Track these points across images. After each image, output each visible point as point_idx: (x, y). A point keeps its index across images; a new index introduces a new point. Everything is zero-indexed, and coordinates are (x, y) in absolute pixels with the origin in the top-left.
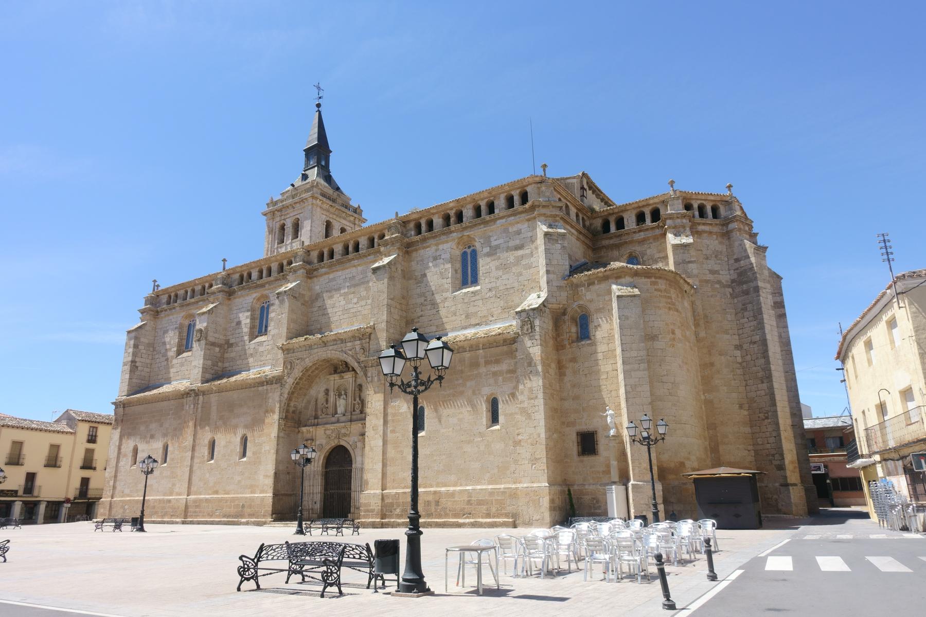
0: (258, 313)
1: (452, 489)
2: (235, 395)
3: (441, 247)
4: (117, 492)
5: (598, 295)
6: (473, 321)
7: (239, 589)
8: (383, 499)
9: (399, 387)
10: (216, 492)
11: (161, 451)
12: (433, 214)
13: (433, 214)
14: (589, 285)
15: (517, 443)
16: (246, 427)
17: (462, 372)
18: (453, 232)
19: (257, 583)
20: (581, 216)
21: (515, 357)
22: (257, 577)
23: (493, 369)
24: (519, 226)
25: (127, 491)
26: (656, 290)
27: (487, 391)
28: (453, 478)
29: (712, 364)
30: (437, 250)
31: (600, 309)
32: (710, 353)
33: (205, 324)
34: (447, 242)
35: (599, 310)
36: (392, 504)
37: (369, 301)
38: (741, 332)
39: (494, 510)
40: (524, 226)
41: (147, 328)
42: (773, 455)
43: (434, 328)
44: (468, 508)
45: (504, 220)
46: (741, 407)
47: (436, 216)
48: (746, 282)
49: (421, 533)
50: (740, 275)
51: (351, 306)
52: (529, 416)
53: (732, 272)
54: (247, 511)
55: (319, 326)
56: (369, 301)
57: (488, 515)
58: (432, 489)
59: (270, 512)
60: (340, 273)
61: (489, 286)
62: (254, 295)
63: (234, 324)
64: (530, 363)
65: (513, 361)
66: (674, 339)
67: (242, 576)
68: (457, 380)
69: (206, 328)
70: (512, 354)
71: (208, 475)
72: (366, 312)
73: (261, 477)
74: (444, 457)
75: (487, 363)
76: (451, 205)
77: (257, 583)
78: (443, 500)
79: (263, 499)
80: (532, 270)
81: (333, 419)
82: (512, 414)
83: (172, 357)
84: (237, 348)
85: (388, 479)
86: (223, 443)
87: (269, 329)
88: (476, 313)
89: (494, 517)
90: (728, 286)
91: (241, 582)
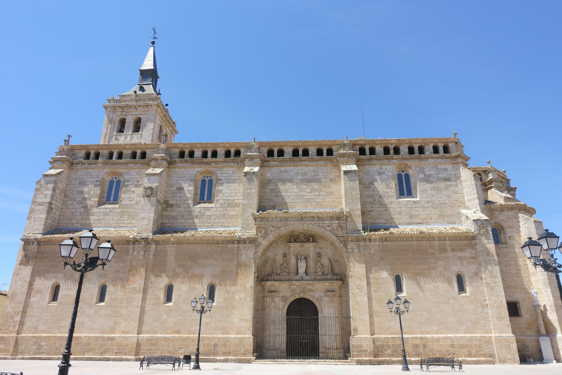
0: (199, 184)
1: (436, 336)
2: (199, 248)
3: (384, 167)
4: (25, 328)
5: (508, 218)
8: (374, 342)
9: (71, 266)
10: (178, 332)
13: (376, 144)
14: (501, 211)
16: (214, 276)
17: (433, 254)
18: (394, 159)
21: (475, 249)
23: (458, 255)
24: (446, 166)
25: (41, 327)
27: (455, 269)
30: (380, 169)
31: (510, 226)
33: (157, 184)
34: (390, 165)
35: (510, 227)
36: (383, 346)
39: (474, 351)
40: (450, 167)
41: (63, 175)
43: (383, 221)
45: (434, 160)
47: (379, 146)
49: (70, 365)
52: (492, 289)
54: (220, 349)
55: (272, 204)
57: (470, 355)
58: (419, 336)
59: (252, 351)
60: (292, 168)
61: (427, 199)
62: (199, 169)
63: (174, 189)
64: (488, 253)
65: (474, 252)
69: (156, 188)
70: (473, 247)
73: (236, 320)
74: (425, 312)
75: (453, 250)
76: (393, 141)
78: (429, 344)
79: (241, 340)
80: (458, 195)
81: (297, 277)
83: (92, 206)
84: (178, 209)
85: (376, 327)
88: (418, 215)
89: (474, 357)
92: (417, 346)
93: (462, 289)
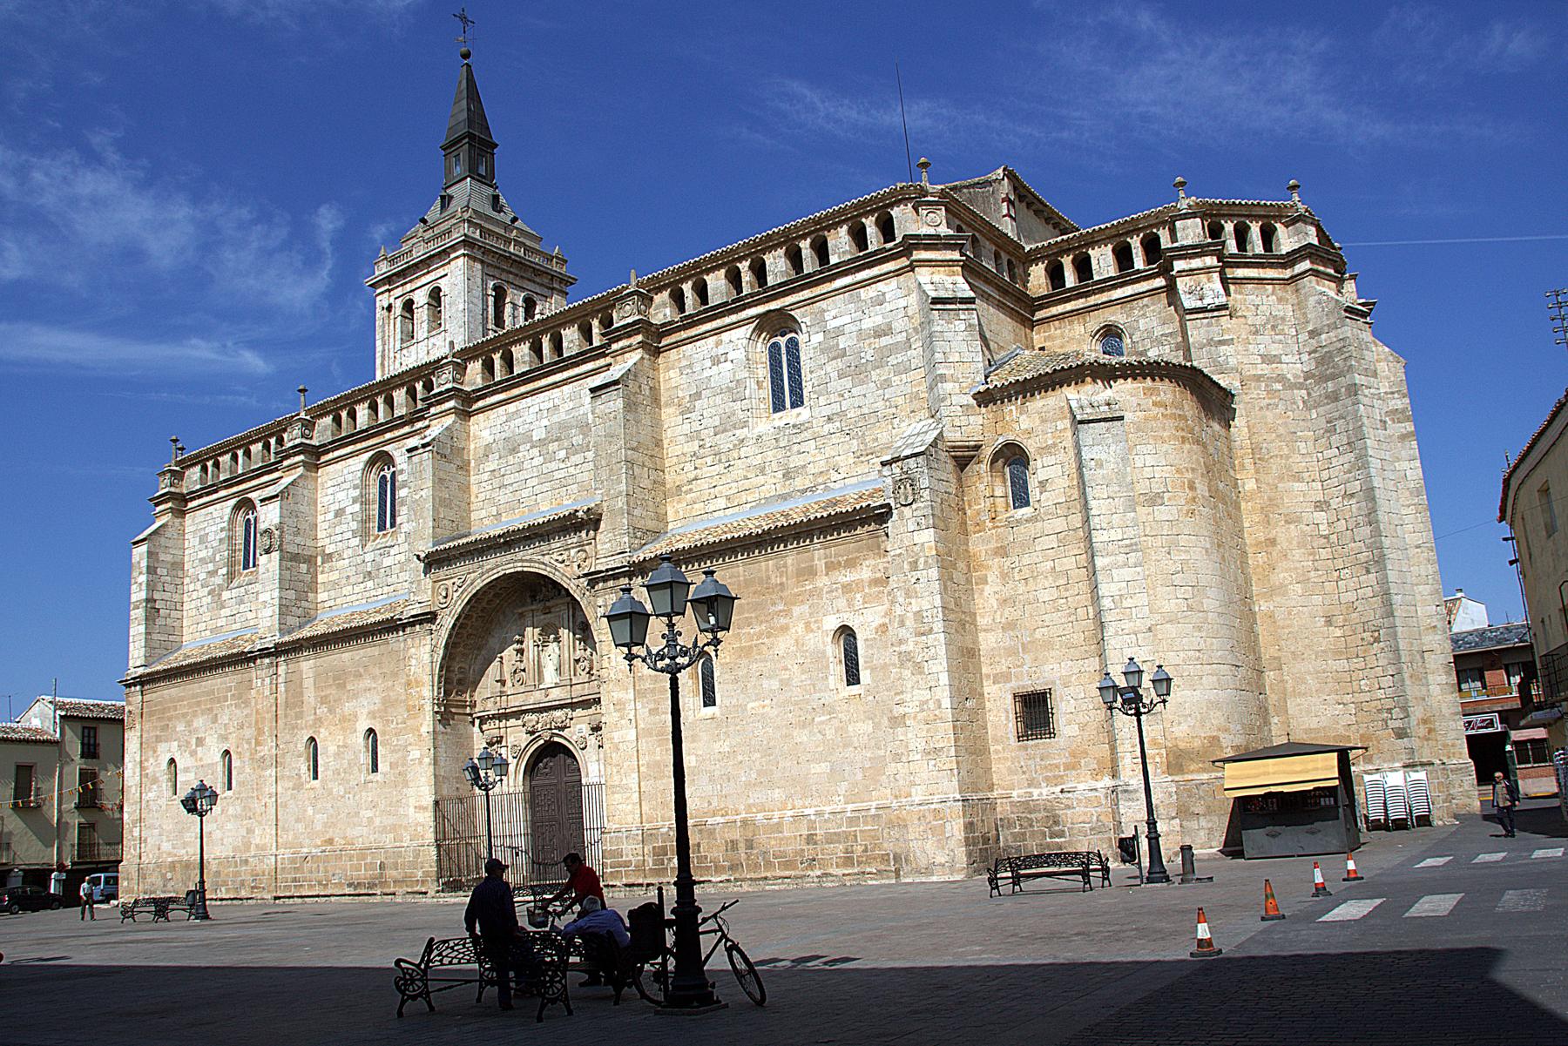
6: (799, 483)
7: (400, 1014)
9: (644, 660)
11: (220, 769)
12: (708, 271)
15: (897, 721)
19: (429, 1003)
20: (1005, 257)
22: (428, 993)
26: (1155, 404)
28: (778, 794)
29: (1273, 542)
30: (718, 344)
32: (1267, 522)
37: (590, 455)
38: (1325, 475)
42: (1389, 711)
44: (809, 852)
46: (1329, 622)
48: (1333, 377)
50: (1321, 362)
51: (553, 466)
52: (918, 668)
53: (1305, 357)
56: (590, 455)
61: (827, 411)
65: (881, 563)
66: (1194, 498)
67: (403, 993)
68: (774, 604)
71: (310, 811)
72: (586, 476)
73: (412, 810)
75: (830, 567)
77: (429, 1003)
78: (762, 838)
82: (885, 667)
86: (332, 749)
87: (399, 520)
90: (1300, 386)
91: (403, 1002)
92: (733, 845)
93: (1511, 563)
